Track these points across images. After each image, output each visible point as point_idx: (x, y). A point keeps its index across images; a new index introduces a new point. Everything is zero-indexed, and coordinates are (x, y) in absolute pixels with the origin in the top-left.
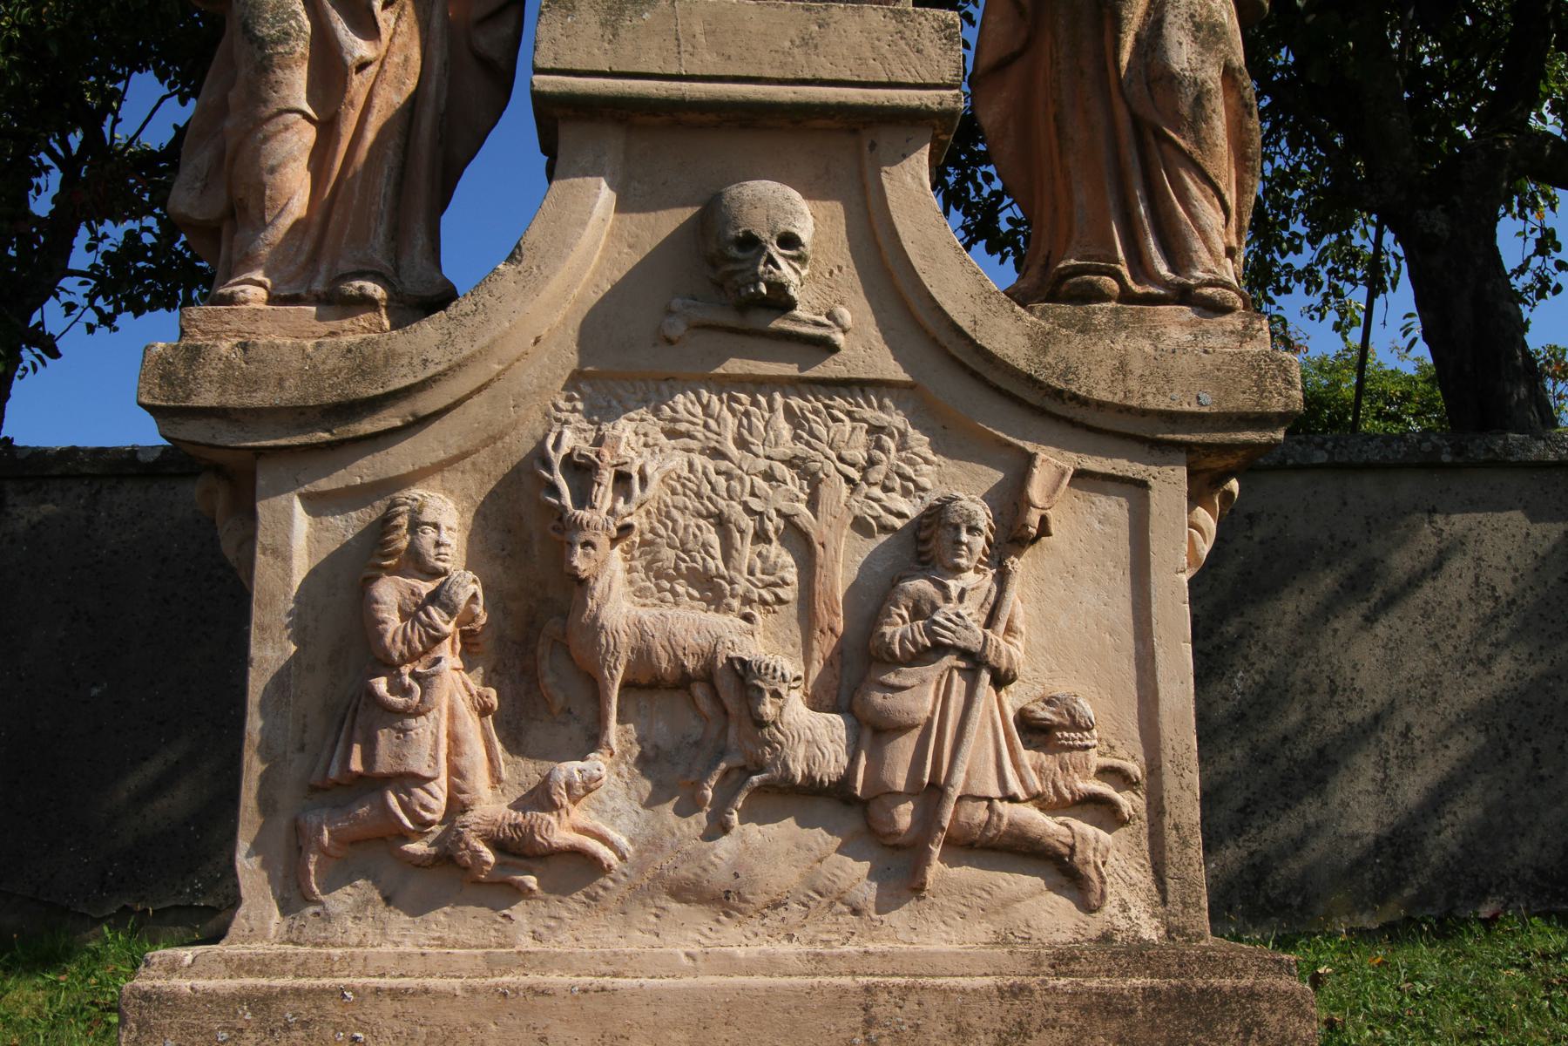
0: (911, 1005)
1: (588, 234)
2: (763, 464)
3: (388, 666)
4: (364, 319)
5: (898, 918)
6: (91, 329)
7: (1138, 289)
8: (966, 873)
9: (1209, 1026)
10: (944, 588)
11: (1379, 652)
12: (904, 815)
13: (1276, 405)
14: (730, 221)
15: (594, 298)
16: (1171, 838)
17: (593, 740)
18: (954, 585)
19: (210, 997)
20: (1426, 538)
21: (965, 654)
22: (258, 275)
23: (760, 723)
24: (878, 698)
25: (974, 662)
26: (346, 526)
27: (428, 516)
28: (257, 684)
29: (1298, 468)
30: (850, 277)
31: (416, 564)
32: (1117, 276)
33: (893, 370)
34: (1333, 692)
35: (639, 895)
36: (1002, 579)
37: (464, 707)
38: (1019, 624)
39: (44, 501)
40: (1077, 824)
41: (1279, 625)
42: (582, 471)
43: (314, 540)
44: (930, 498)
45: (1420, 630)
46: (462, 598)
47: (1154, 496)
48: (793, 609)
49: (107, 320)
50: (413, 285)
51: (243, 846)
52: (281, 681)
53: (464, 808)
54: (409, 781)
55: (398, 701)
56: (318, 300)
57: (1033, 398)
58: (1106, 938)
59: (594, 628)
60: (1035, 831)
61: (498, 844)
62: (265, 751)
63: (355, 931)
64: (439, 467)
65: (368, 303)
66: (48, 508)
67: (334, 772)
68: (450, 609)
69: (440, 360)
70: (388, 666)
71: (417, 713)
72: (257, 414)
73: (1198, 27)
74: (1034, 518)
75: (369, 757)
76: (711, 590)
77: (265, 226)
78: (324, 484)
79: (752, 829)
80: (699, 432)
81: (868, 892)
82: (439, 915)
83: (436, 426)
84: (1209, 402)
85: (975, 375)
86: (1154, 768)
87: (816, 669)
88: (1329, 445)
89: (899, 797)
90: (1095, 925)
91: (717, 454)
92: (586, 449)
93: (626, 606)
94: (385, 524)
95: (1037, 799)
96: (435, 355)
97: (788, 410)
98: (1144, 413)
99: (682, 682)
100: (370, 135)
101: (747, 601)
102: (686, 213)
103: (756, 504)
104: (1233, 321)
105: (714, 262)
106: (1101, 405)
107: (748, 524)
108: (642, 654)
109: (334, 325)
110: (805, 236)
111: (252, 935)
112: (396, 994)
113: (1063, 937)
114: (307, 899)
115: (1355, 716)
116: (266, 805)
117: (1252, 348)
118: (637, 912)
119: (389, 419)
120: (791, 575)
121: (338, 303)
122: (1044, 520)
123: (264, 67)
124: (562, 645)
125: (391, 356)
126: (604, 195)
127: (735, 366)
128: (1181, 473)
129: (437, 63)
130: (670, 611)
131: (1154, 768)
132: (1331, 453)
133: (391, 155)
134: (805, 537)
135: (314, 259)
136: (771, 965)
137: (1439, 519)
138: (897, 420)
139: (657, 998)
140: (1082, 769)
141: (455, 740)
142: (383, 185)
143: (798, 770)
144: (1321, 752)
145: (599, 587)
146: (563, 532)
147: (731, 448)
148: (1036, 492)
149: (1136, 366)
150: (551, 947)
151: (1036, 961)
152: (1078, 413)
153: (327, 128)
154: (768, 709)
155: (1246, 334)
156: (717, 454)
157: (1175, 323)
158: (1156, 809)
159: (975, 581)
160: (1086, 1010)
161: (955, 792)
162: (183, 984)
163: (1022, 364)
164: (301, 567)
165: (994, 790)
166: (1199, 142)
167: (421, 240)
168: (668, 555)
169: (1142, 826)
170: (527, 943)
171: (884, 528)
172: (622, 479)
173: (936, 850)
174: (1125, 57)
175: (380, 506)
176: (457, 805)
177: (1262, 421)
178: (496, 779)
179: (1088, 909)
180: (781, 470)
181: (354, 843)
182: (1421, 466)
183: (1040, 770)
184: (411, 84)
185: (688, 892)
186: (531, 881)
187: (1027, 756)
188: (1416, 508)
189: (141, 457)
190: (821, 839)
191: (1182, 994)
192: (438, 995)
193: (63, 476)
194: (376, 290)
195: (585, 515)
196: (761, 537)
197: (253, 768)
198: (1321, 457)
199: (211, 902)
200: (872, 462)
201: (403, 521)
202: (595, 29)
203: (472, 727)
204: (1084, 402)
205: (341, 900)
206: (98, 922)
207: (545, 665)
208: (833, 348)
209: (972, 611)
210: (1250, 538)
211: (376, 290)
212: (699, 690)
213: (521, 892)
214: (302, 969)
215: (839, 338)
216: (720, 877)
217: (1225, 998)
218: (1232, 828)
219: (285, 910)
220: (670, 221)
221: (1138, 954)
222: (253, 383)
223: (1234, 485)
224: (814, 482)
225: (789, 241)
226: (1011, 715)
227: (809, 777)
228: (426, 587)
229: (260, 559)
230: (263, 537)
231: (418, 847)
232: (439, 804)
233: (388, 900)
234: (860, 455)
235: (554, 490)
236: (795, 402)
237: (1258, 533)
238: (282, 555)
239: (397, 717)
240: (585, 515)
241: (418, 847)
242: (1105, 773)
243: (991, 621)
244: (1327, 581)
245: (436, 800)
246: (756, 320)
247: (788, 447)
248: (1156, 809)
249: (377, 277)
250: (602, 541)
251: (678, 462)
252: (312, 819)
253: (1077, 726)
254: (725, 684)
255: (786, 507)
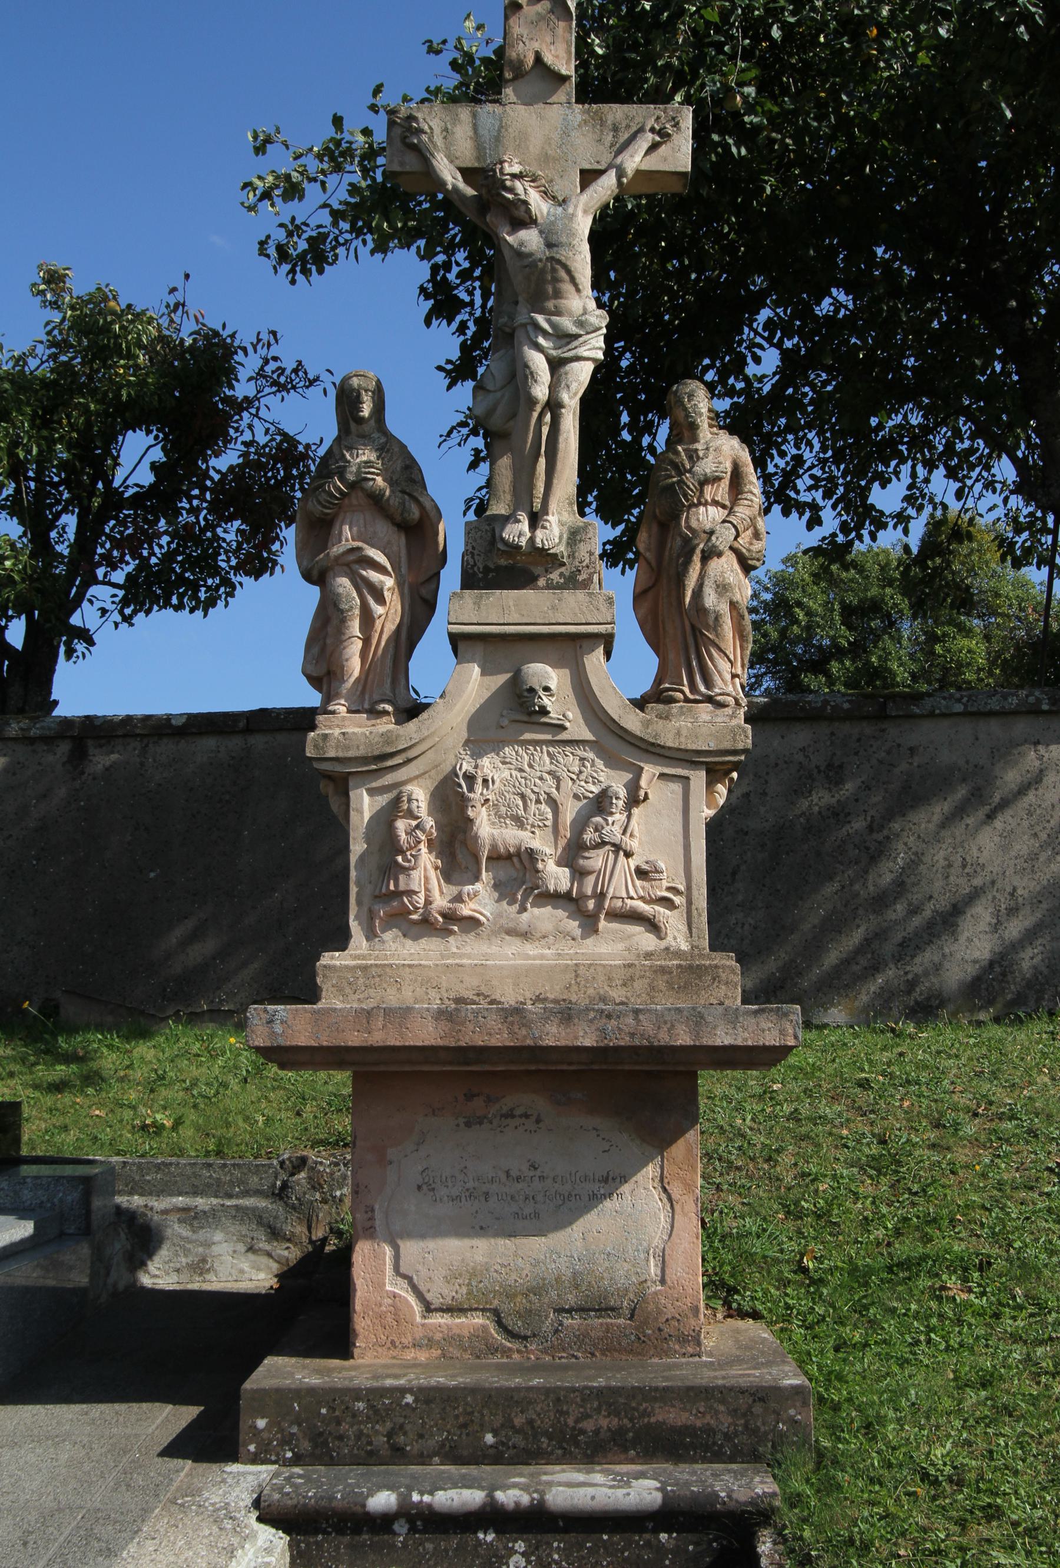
0: (592, 970)
1: (471, 685)
2: (539, 774)
3: (402, 852)
4: (385, 719)
5: (589, 941)
6: (116, 625)
7: (691, 697)
8: (615, 926)
9: (700, 977)
10: (606, 820)
11: (997, 839)
12: (591, 904)
13: (740, 746)
14: (524, 682)
15: (473, 710)
16: (695, 913)
17: (477, 878)
18: (610, 819)
19: (347, 967)
20: (1031, 759)
21: (614, 845)
22: (343, 702)
23: (537, 871)
24: (581, 862)
25: (617, 848)
26: (383, 800)
27: (414, 796)
28: (353, 859)
29: (944, 715)
30: (572, 699)
31: (410, 814)
32: (682, 692)
33: (589, 736)
34: (964, 866)
35: (495, 933)
36: (629, 817)
37: (429, 866)
38: (636, 833)
39: (112, 752)
40: (657, 908)
41: (929, 822)
42: (470, 779)
43: (371, 805)
44: (603, 786)
45: (1025, 824)
46: (428, 827)
47: (692, 782)
48: (550, 829)
49: (127, 619)
50: (403, 704)
51: (352, 917)
52: (362, 858)
53: (431, 903)
54: (411, 893)
55: (406, 864)
56: (367, 712)
57: (643, 746)
58: (667, 949)
59: (476, 837)
60: (640, 910)
61: (444, 916)
62: (358, 883)
63: (393, 946)
64: (417, 777)
65: (385, 713)
66: (114, 757)
67: (384, 890)
68: (424, 831)
69: (416, 738)
70: (402, 852)
71: (413, 869)
72: (350, 759)
73: (718, 586)
74: (642, 793)
75: (396, 885)
76: (519, 822)
77: (344, 682)
78: (374, 785)
79: (536, 910)
80: (514, 762)
81: (578, 932)
82: (423, 941)
83: (415, 762)
84: (713, 746)
85: (621, 737)
86: (689, 888)
87: (559, 851)
88: (965, 700)
89: (589, 898)
90: (663, 944)
91: (521, 770)
92: (473, 771)
93: (487, 829)
94: (397, 800)
95: (641, 898)
96: (414, 736)
97: (548, 753)
98: (687, 751)
99: (509, 857)
100: (383, 643)
101: (533, 826)
102: (509, 675)
103: (536, 789)
104: (728, 711)
105: (520, 696)
106: (670, 748)
107: (533, 797)
108: (494, 847)
109: (373, 722)
110: (553, 687)
111: (357, 948)
112: (410, 966)
113: (651, 948)
114: (376, 936)
115: (977, 882)
116: (359, 903)
117: (734, 722)
118: (493, 939)
119: (398, 760)
120: (550, 816)
121: (375, 713)
122: (646, 794)
123: (343, 621)
124: (464, 843)
125: (398, 736)
126: (476, 670)
127: (527, 736)
128: (704, 773)
129: (407, 607)
130: (504, 831)
131: (689, 888)
132: (965, 705)
133: (391, 650)
134: (555, 801)
135: (363, 692)
136: (542, 957)
137: (1041, 748)
138: (591, 755)
139: (502, 967)
140: (660, 888)
141: (426, 878)
142: (389, 662)
143: (552, 888)
144: (954, 906)
145: (477, 822)
146: (463, 802)
147: (526, 768)
148: (643, 783)
149: (684, 732)
150: (463, 951)
151: (638, 956)
152: (662, 751)
153: (366, 641)
154: (540, 866)
155: (733, 716)
156: (521, 770)
157: (705, 710)
158: (689, 902)
159: (619, 817)
160: (655, 972)
161: (609, 896)
162: (338, 963)
163: (638, 733)
164: (367, 816)
165: (624, 895)
166: (717, 636)
167: (403, 682)
168: (503, 809)
169: (684, 909)
170: (455, 950)
171: (585, 798)
172: (485, 781)
173: (602, 917)
174: (688, 600)
175: (395, 793)
176: (428, 902)
177: (735, 752)
178: (441, 892)
179: (661, 939)
180: (546, 776)
181: (392, 916)
182: (1029, 712)
183: (643, 888)
184: (398, 620)
185: (512, 932)
186: (456, 928)
187: (638, 883)
188: (1026, 741)
189: (173, 722)
190: (561, 913)
191: (691, 967)
192: (425, 966)
193: (125, 736)
194: (389, 708)
195: (471, 795)
196: (538, 802)
197: (353, 890)
198: (959, 708)
199: (232, 1007)
200: (581, 772)
201: (405, 799)
202: (471, 605)
203: (432, 874)
204: (663, 747)
205: (388, 936)
206: (165, 1019)
207: (458, 852)
208: (565, 728)
209: (617, 829)
210: (911, 764)
211: (389, 708)
212: (515, 860)
213: (451, 932)
214: (377, 958)
215: (567, 724)
216: (524, 927)
217: (706, 968)
218: (893, 956)
219: (368, 939)
220: (502, 679)
221: (678, 954)
222: (347, 748)
223: (735, 775)
224: (558, 780)
225: (547, 689)
226: (633, 868)
227: (556, 891)
228: (414, 823)
229: (352, 813)
230: (353, 805)
231: (414, 917)
232: (422, 901)
233: (405, 936)
234: (576, 769)
235: (460, 786)
236: (551, 749)
237: (916, 761)
238: (360, 812)
239: (406, 870)
240: (471, 795)
241: (414, 917)
242: (669, 889)
243: (624, 833)
244: (962, 792)
245: (421, 899)
246: (535, 718)
247: (548, 767)
248: (689, 902)
249: (389, 702)
250: (478, 805)
251: (506, 774)
252: (376, 907)
253: (657, 871)
254: (525, 857)
255: (547, 790)
